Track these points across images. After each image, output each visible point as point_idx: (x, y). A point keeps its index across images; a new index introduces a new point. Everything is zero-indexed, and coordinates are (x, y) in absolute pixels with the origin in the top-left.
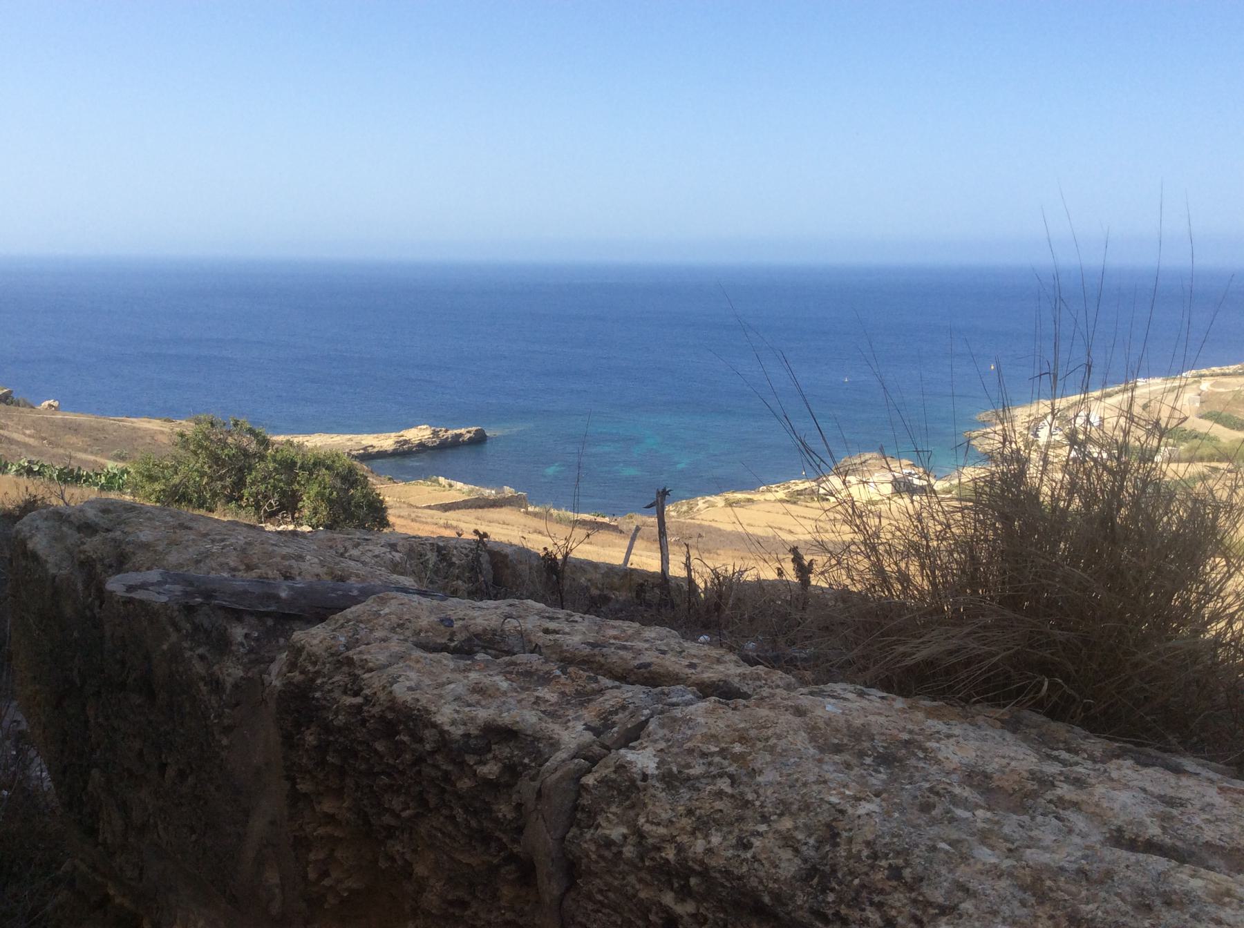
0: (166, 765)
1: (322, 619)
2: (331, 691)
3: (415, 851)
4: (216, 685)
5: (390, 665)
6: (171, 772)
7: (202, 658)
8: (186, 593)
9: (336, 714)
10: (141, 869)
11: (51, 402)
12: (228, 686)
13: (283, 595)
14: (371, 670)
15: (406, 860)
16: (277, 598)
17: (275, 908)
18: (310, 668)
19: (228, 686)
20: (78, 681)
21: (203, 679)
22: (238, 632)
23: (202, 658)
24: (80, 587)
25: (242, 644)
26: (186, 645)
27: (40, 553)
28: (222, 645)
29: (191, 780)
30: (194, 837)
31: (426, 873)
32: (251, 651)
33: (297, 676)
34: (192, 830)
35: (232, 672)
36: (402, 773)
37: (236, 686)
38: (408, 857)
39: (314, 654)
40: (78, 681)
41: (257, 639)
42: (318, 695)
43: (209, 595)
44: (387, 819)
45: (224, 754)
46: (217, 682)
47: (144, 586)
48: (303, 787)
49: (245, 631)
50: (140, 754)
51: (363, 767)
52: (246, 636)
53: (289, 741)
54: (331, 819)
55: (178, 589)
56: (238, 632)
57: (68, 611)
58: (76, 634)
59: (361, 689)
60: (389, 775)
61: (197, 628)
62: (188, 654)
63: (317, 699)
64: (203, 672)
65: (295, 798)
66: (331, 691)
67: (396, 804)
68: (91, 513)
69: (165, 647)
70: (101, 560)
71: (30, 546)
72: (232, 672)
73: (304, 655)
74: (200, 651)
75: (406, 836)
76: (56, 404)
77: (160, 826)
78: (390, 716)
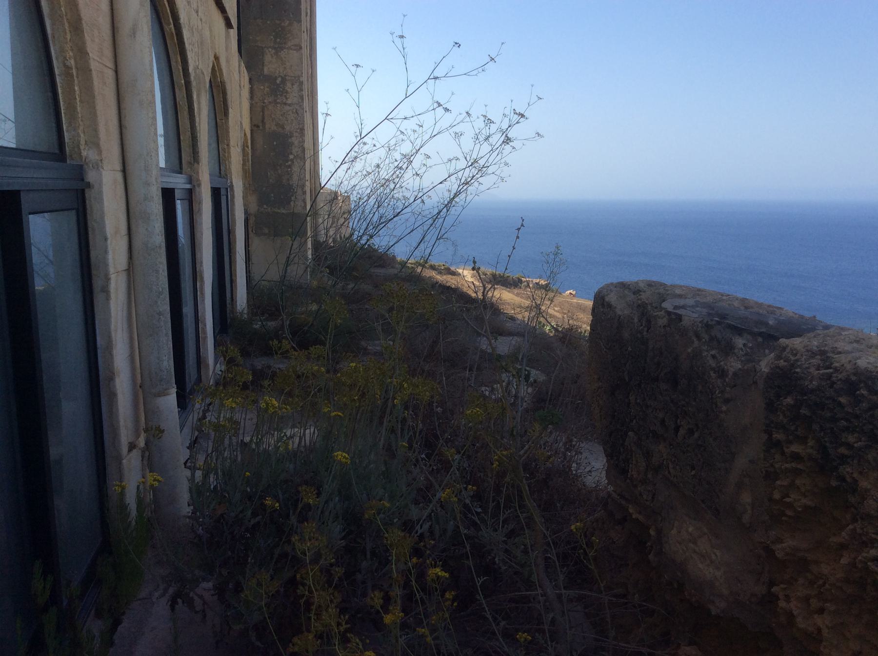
0: (679, 427)
1: (800, 336)
2: (809, 368)
3: (861, 473)
4: (722, 373)
5: (852, 352)
6: (682, 432)
7: (714, 357)
8: (709, 314)
9: (811, 381)
10: (654, 494)
11: (571, 291)
12: (731, 373)
13: (771, 322)
14: (840, 353)
15: (853, 478)
16: (767, 324)
17: (746, 518)
18: (793, 358)
19: (731, 373)
20: (627, 379)
21: (713, 369)
22: (739, 342)
23: (714, 357)
24: (636, 320)
25: (742, 349)
26: (705, 348)
27: (613, 303)
28: (728, 349)
29: (696, 435)
30: (693, 472)
31: (869, 487)
32: (746, 354)
33: (782, 363)
34: (693, 468)
35: (734, 365)
36: (857, 417)
37: (735, 374)
38: (855, 475)
39: (795, 349)
40: (627, 379)
41: (751, 348)
42: (798, 370)
43: (723, 317)
44: (843, 450)
45: (722, 415)
46: (723, 371)
47: (683, 307)
48: (778, 436)
49: (744, 342)
50: (663, 422)
51: (829, 414)
52: (744, 345)
53: (771, 407)
54: (796, 457)
55: (705, 311)
56: (739, 342)
57: (626, 335)
58: (630, 349)
59: (832, 364)
60: (847, 420)
61: (712, 339)
62: (705, 354)
63: (797, 373)
64: (714, 365)
65: (772, 445)
66: (809, 368)
67: (851, 439)
68: (642, 285)
69: (689, 350)
70: (651, 304)
71: (607, 299)
72: (734, 365)
73: (788, 350)
74: (713, 352)
75: (855, 461)
76: (574, 293)
77: (671, 466)
78: (854, 378)
